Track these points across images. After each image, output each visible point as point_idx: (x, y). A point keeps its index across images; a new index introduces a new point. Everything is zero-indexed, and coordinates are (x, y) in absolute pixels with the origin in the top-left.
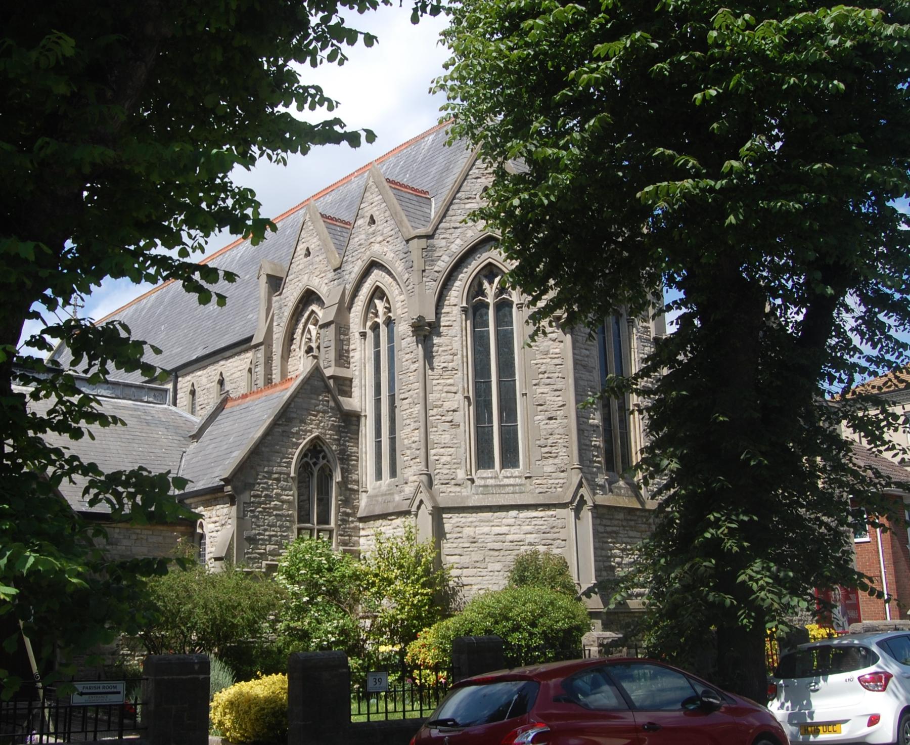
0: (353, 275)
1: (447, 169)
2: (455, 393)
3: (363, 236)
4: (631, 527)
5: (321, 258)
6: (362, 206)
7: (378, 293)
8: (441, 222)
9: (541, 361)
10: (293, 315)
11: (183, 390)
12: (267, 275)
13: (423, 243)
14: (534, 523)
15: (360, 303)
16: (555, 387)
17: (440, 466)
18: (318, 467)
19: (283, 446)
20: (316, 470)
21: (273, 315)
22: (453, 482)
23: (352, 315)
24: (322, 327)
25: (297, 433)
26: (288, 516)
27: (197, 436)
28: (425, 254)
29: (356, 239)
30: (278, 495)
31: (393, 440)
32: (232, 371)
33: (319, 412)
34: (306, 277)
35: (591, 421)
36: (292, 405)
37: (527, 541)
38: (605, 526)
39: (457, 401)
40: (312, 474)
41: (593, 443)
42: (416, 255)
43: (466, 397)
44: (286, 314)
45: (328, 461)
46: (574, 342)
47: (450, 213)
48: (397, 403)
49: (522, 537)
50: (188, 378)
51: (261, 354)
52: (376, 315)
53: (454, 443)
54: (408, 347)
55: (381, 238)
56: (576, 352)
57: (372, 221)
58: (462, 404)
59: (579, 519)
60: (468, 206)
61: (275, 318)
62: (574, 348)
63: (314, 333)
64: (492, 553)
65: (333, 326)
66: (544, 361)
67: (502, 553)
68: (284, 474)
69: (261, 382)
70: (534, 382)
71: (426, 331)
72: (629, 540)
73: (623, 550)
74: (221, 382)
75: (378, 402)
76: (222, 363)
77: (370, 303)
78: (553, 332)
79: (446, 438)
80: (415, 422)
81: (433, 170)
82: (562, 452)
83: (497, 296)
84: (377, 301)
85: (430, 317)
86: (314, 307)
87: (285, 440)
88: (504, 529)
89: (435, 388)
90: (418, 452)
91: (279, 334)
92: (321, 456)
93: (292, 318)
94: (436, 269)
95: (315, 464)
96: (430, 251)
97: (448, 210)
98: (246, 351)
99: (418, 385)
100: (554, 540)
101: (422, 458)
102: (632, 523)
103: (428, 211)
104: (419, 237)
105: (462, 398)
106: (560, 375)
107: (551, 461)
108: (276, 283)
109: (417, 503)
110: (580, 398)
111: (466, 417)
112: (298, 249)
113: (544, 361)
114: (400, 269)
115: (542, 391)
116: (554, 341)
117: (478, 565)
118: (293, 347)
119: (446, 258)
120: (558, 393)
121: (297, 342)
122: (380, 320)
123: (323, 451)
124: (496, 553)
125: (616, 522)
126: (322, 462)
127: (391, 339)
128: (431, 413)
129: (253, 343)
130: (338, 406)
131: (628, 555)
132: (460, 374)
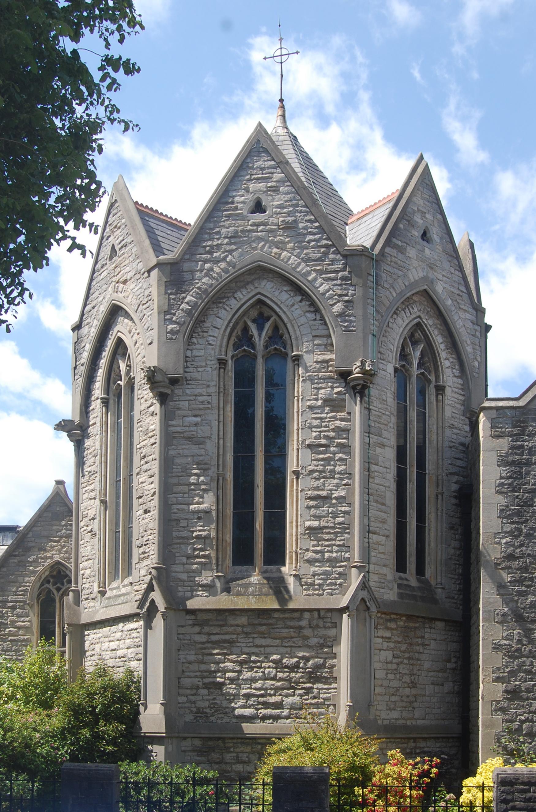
19: (20, 576)
25: (34, 561)
26: (24, 640)
30: (13, 622)
33: (61, 537)
35: (192, 507)
36: (30, 534)
38: (209, 634)
41: (195, 534)
59: (151, 628)
68: (20, 601)
73: (241, 663)
87: (21, 569)
102: (263, 629)
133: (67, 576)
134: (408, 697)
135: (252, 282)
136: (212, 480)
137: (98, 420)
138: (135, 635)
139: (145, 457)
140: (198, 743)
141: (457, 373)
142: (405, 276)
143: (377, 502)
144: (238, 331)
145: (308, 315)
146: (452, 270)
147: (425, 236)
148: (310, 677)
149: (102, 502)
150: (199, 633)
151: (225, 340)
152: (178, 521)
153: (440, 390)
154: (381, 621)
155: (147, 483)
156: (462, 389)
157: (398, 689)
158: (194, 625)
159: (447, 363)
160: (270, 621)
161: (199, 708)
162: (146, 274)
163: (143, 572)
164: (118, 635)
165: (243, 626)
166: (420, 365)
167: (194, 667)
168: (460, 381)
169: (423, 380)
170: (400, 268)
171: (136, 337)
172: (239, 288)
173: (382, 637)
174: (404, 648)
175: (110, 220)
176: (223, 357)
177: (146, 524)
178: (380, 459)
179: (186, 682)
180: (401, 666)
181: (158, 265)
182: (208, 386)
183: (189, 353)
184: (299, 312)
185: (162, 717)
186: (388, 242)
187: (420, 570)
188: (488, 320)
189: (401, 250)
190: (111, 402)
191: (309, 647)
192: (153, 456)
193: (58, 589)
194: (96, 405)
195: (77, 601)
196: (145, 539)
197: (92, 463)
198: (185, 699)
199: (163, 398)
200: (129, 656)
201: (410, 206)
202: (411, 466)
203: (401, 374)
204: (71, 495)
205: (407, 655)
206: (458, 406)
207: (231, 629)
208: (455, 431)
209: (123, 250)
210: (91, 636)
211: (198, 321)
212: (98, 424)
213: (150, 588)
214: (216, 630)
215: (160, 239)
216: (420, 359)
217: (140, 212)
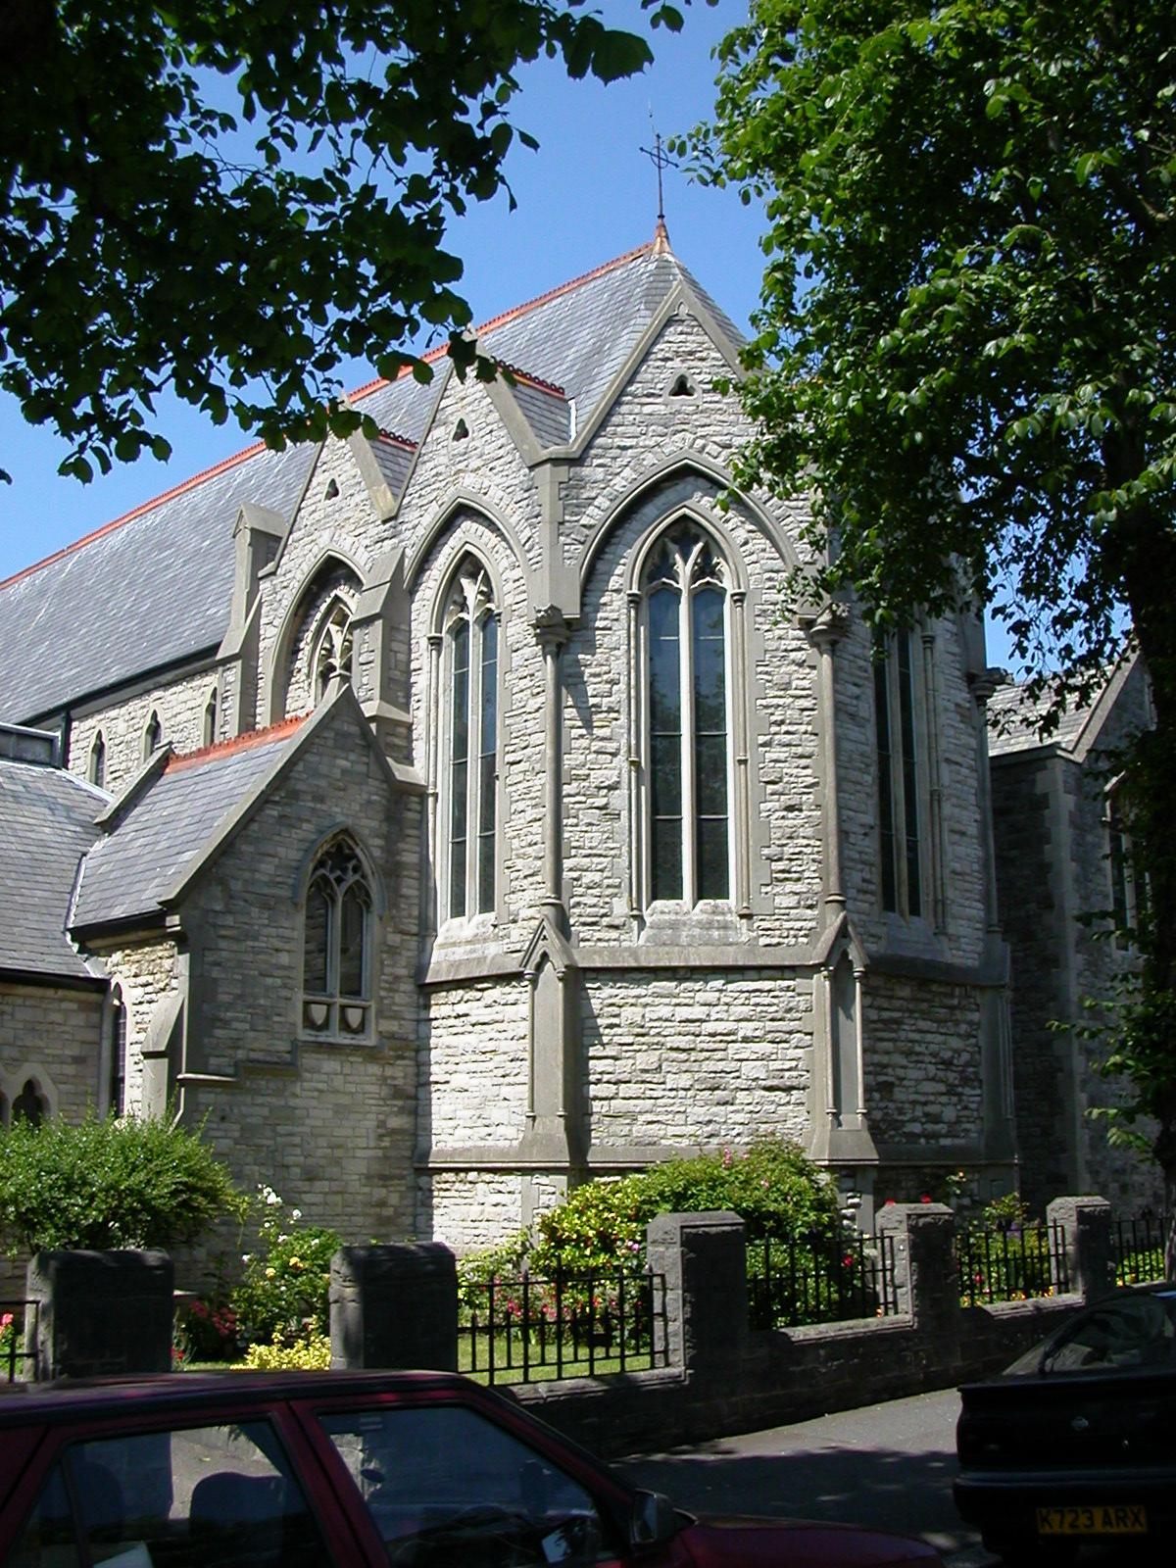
0: (421, 531)
1: (598, 352)
2: (613, 755)
3: (444, 460)
4: (922, 1012)
5: (357, 498)
6: (443, 404)
7: (469, 564)
8: (596, 435)
9: (775, 701)
10: (300, 605)
11: (81, 744)
12: (252, 530)
13: (563, 472)
14: (753, 1001)
15: (433, 584)
16: (799, 750)
17: (581, 890)
18: (345, 886)
20: (340, 892)
21: (260, 605)
22: (605, 921)
23: (414, 606)
24: (355, 625)
27: (111, 825)
28: (563, 494)
29: (430, 465)
31: (488, 842)
32: (176, 710)
34: (326, 535)
37: (741, 1034)
38: (881, 1009)
39: (618, 769)
40: (333, 901)
42: (545, 494)
43: (632, 763)
44: (285, 602)
45: (364, 876)
46: (836, 671)
47: (615, 419)
48: (500, 769)
49: (732, 1026)
50: (90, 722)
51: (234, 674)
52: (463, 606)
53: (609, 846)
54: (525, 667)
55: (479, 463)
56: (838, 687)
57: (462, 432)
58: (625, 776)
60: (647, 409)
61: (264, 610)
62: (836, 679)
63: (338, 640)
64: (674, 1055)
65: (379, 623)
66: (781, 701)
67: (693, 1056)
69: (232, 729)
70: (762, 739)
71: (563, 636)
74: (154, 731)
75: (460, 769)
76: (157, 694)
77: (452, 585)
78: (800, 649)
79: (594, 838)
80: (535, 806)
81: (571, 354)
82: (810, 871)
83: (695, 577)
84: (465, 582)
85: (571, 611)
86: (342, 591)
87: (285, 833)
88: (698, 1012)
89: (575, 744)
90: (539, 863)
91: (271, 638)
92: (350, 866)
93: (295, 614)
94: (585, 521)
95: (339, 880)
96: (573, 487)
97: (610, 414)
98: (204, 672)
99: (543, 739)
100: (790, 1033)
101: (547, 874)
102: (924, 1006)
103: (565, 422)
104: (556, 461)
105: (626, 765)
106: (810, 728)
107: (789, 887)
108: (267, 547)
109: (536, 958)
110: (843, 772)
111: (629, 800)
112: (315, 481)
113: (781, 701)
114: (514, 520)
115: (774, 756)
116: (801, 665)
117: (647, 1077)
118: (298, 664)
119: (603, 502)
120: (803, 762)
121: (304, 655)
122: (470, 617)
123: (355, 856)
124: (684, 1056)
125: (898, 1003)
126: (351, 878)
127: (489, 651)
128: (566, 789)
129: (219, 656)
130: (388, 775)
132: (623, 718)
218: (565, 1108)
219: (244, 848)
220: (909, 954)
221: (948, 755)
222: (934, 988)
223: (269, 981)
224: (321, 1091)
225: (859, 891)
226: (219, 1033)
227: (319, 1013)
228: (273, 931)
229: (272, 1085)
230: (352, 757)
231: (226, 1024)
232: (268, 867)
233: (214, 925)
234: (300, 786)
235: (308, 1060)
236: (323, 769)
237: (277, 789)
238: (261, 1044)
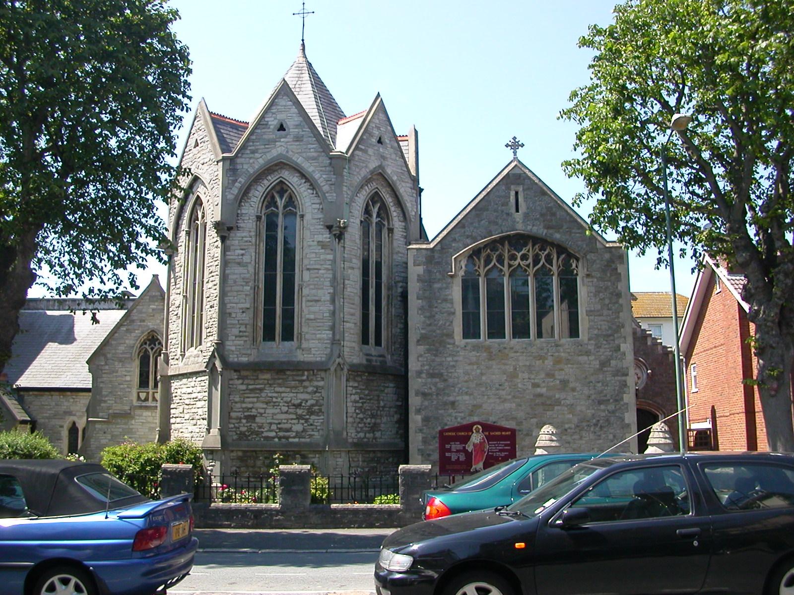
72: (276, 395)
102: (280, 381)
131: (274, 406)
133: (158, 339)
134: (369, 424)
135: (276, 171)
136: (251, 288)
137: (183, 244)
138: (203, 384)
139: (211, 272)
140: (240, 454)
141: (402, 219)
142: (366, 167)
143: (349, 303)
144: (269, 198)
145: (309, 191)
146: (397, 158)
147: (380, 141)
148: (308, 412)
149: (184, 296)
150: (242, 384)
151: (260, 205)
152: (230, 314)
153: (391, 231)
154: (351, 377)
155: (212, 289)
156: (405, 229)
157: (362, 419)
158: (238, 379)
159: (395, 214)
160: (285, 377)
161: (241, 432)
162: (216, 163)
163: (209, 344)
164: (192, 384)
165: (268, 380)
166: (378, 215)
167: (238, 405)
168: (403, 224)
169: (380, 226)
170: (363, 162)
171: (208, 198)
172: (270, 174)
173: (352, 387)
174: (367, 392)
175: (196, 123)
176: (259, 214)
177: (211, 315)
178: (351, 276)
179: (233, 415)
180: (365, 405)
181: (224, 159)
182: (250, 232)
183: (239, 212)
184: (304, 189)
185: (219, 438)
186: (357, 148)
187: (378, 343)
188: (421, 185)
189: (365, 151)
190: (192, 233)
191: (307, 393)
192: (217, 273)
193: (152, 349)
194: (183, 235)
195: (167, 361)
196: (211, 323)
197: (180, 271)
198: (232, 426)
199: (223, 239)
200: (199, 397)
201: (371, 124)
202: (372, 278)
203: (365, 225)
204: (164, 285)
205: (368, 397)
206: (402, 239)
207: (261, 382)
208: (400, 255)
209: (202, 144)
210: (175, 384)
211: (245, 194)
212: (184, 246)
213: (213, 356)
214: (252, 382)
215: (225, 136)
216: (378, 213)
217: (213, 120)
218: (220, 426)
219: (113, 342)
220: (271, 359)
221: (308, 267)
222: (288, 373)
223: (122, 386)
224: (143, 423)
225: (236, 337)
226: (103, 405)
227: (143, 396)
228: (124, 369)
229: (123, 421)
230: (156, 304)
231: (105, 402)
232: (122, 348)
233: (102, 370)
234: (135, 318)
235: (138, 412)
236: (144, 310)
237: (126, 320)
238: (118, 408)
